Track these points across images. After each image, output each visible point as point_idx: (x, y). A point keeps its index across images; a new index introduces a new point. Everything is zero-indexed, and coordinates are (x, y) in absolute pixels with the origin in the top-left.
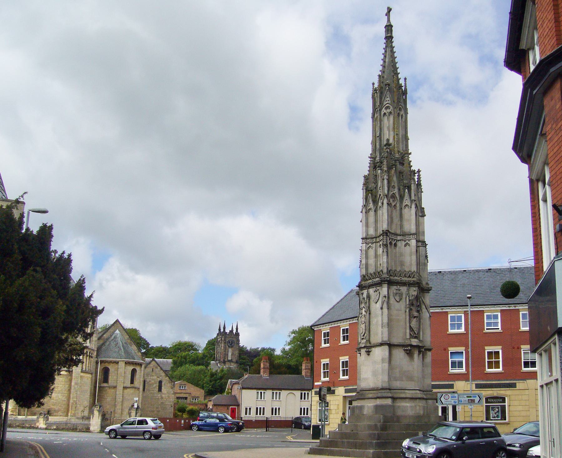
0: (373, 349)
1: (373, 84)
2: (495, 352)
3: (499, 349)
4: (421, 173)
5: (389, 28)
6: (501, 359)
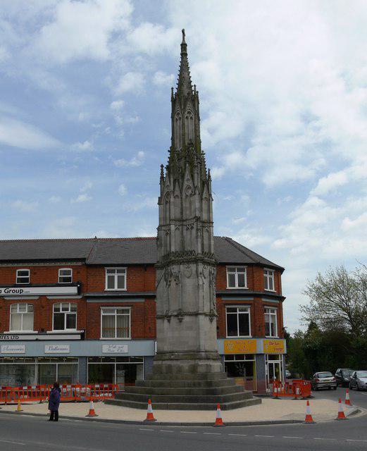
1: (172, 89)
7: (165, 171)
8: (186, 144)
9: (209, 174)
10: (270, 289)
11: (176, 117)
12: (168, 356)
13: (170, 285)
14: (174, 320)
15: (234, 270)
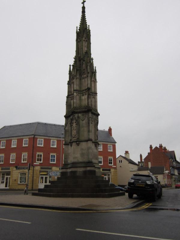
0: (81, 143)
1: (77, 27)
2: (40, 155)
3: (42, 154)
4: (96, 68)
5: (84, 8)
6: (42, 158)
7: (72, 67)
8: (84, 53)
9: (95, 68)
11: (79, 40)
12: (69, 166)
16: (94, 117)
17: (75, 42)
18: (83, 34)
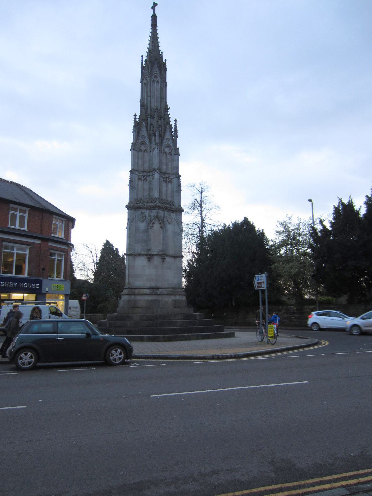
1: (142, 56)
9: (176, 124)
10: (60, 235)
11: (144, 81)
13: (153, 226)
14: (157, 260)
15: (16, 210)
16: (173, 215)
17: (140, 84)
18: (154, 68)
